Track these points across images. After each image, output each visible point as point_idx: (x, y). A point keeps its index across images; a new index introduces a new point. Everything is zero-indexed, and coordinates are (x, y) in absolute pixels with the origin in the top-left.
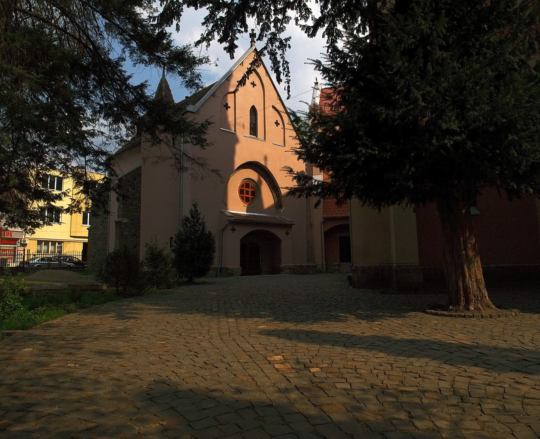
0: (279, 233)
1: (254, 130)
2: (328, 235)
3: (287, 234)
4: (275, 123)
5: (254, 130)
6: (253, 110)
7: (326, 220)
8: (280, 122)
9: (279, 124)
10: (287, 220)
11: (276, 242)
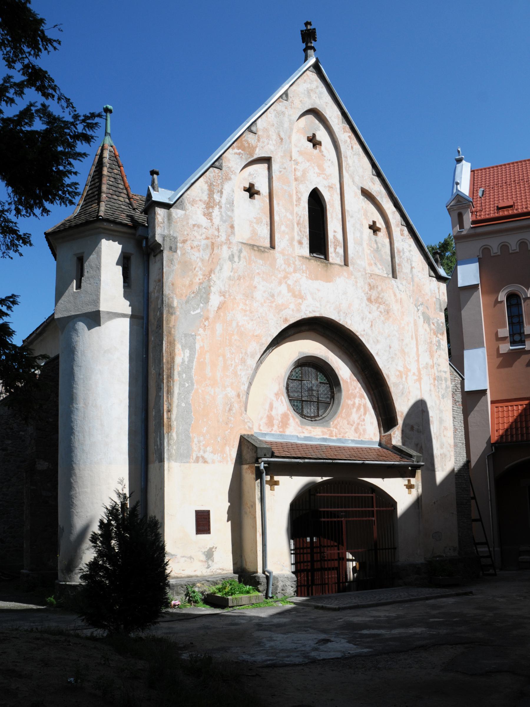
1: (318, 243)
4: (371, 227)
5: (318, 243)
6: (316, 200)
8: (322, 135)
9: (379, 230)
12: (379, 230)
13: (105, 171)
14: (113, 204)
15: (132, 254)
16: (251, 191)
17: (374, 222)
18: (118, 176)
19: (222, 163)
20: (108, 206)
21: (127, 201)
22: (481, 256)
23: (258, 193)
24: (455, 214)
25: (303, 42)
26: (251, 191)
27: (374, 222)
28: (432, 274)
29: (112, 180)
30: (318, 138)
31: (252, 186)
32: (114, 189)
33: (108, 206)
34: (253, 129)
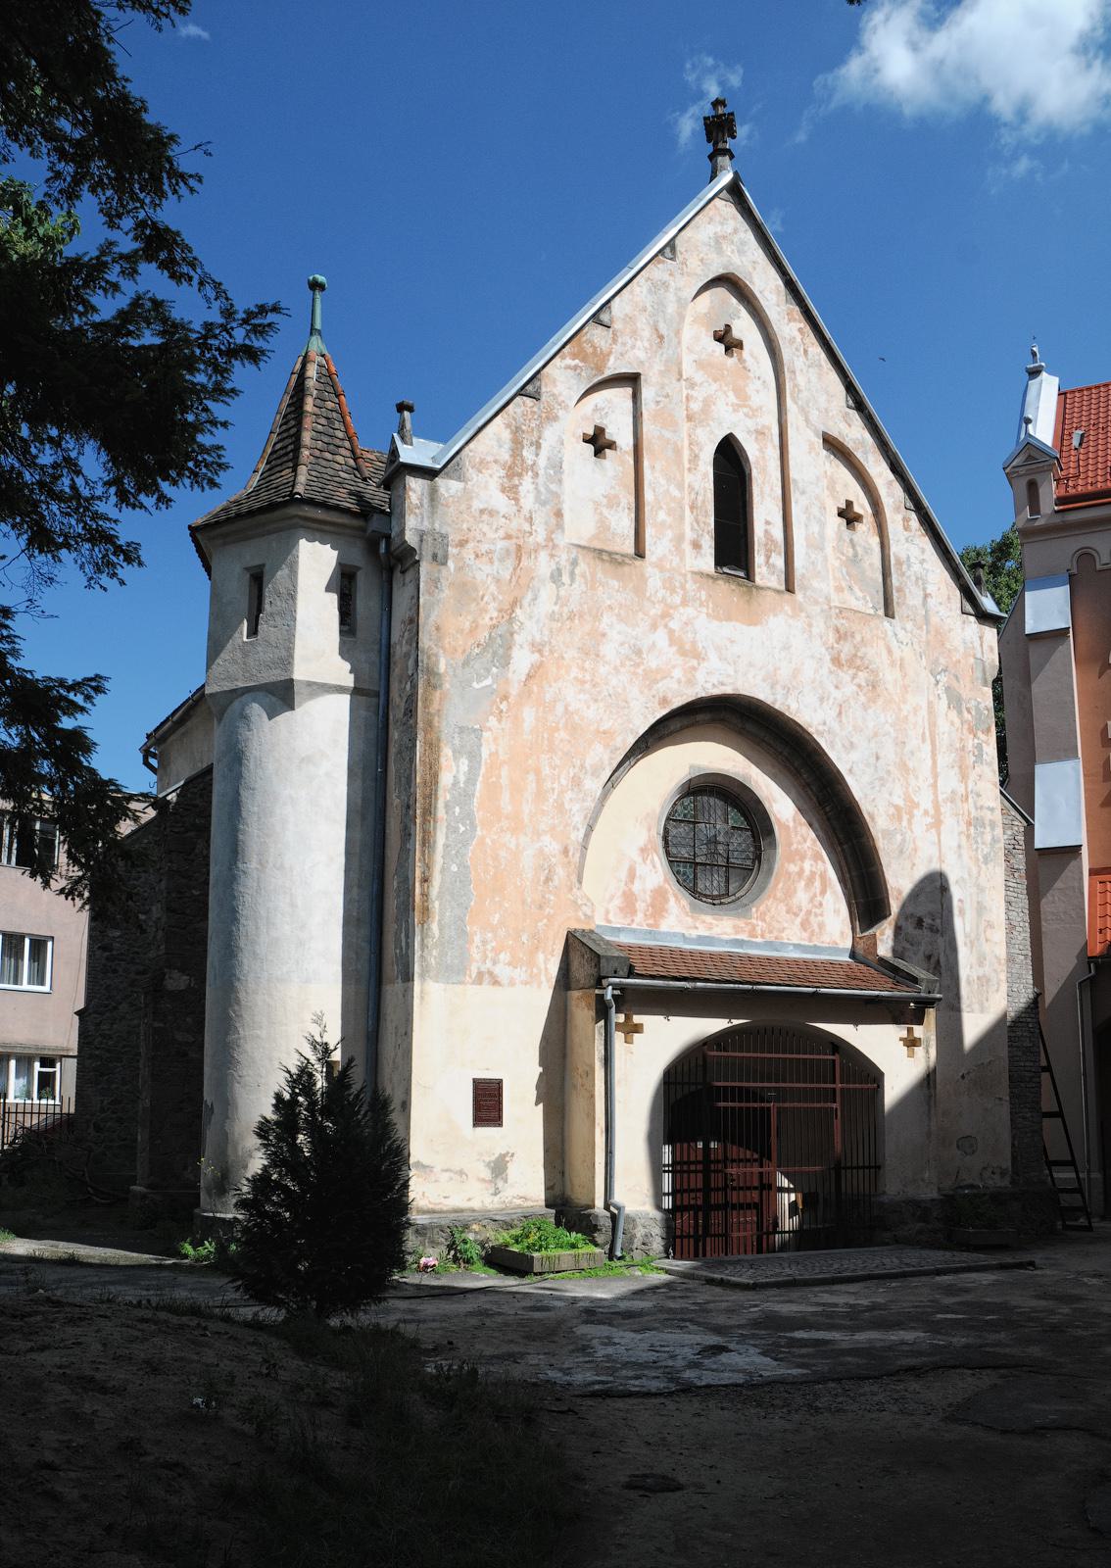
1: (733, 546)
4: (841, 514)
5: (733, 546)
6: (730, 461)
8: (744, 327)
9: (858, 518)
12: (858, 518)
13: (309, 405)
14: (324, 470)
15: (359, 568)
16: (599, 442)
17: (849, 504)
18: (335, 415)
19: (540, 388)
20: (314, 473)
21: (351, 462)
22: (1074, 571)
23: (611, 445)
24: (1023, 483)
25: (709, 141)
26: (599, 442)
27: (849, 504)
28: (969, 608)
29: (323, 421)
30: (736, 333)
31: (599, 431)
32: (326, 439)
33: (314, 473)
34: (604, 317)
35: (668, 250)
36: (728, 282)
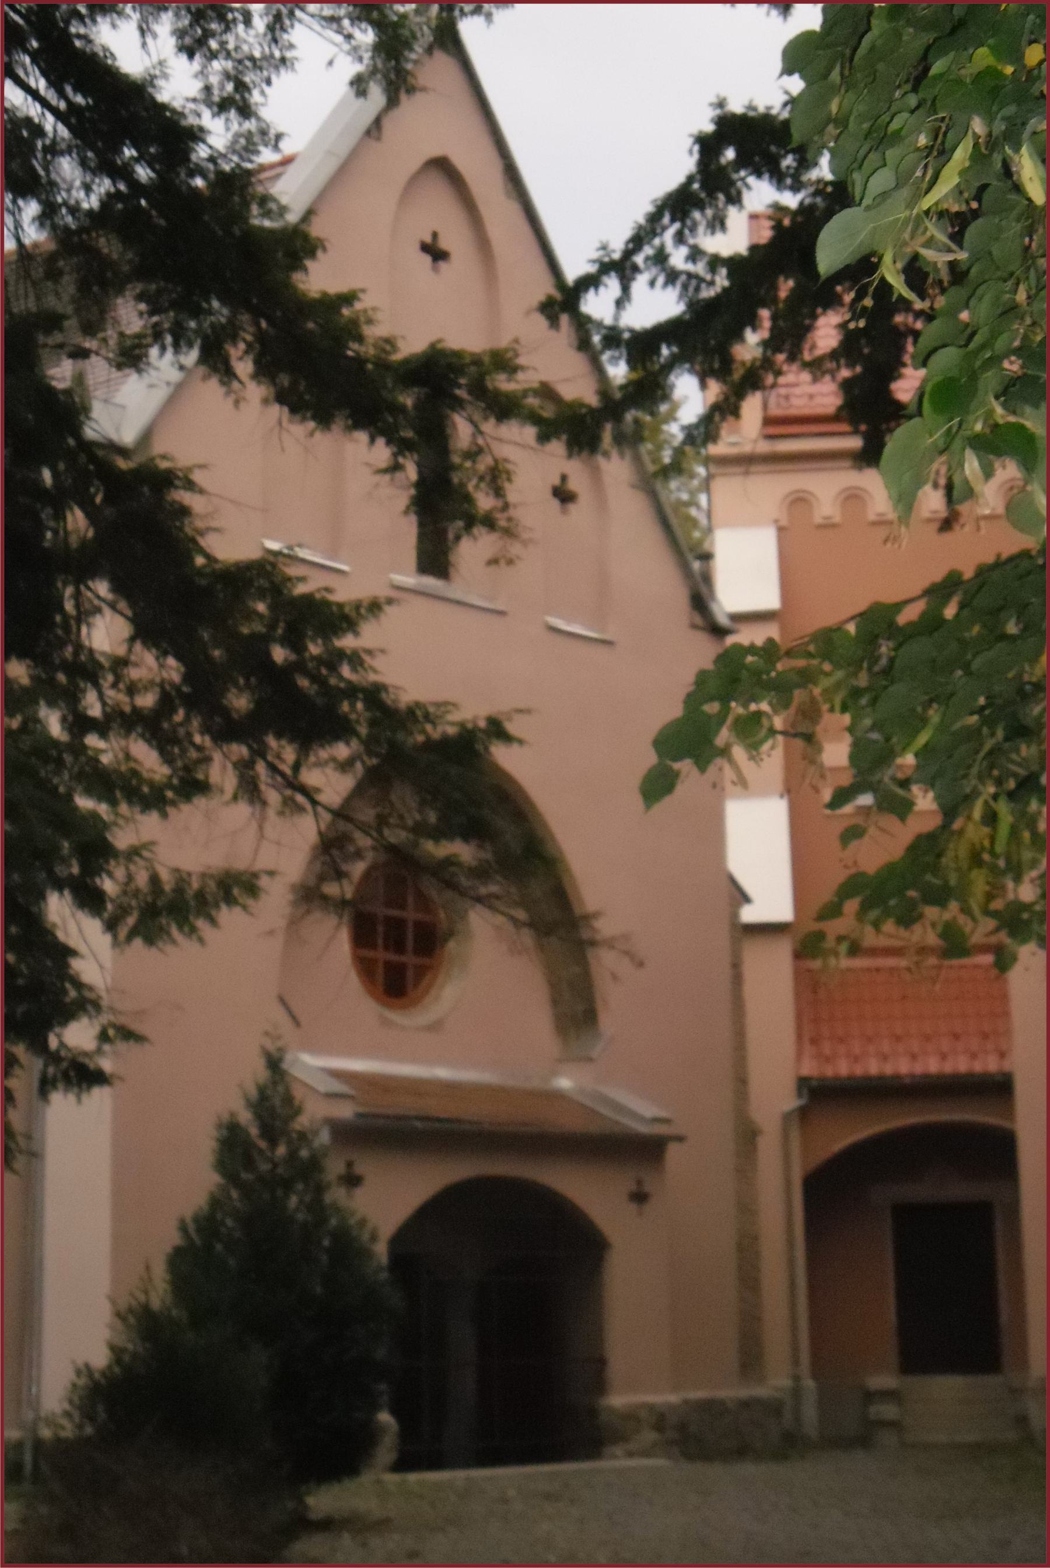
0: (594, 1194)
2: (830, 1192)
3: (640, 1197)
7: (820, 1096)
8: (455, 238)
10: (640, 1109)
11: (579, 1245)
17: (564, 478)
22: (784, 522)
28: (698, 620)
30: (444, 244)
35: (374, 133)
36: (442, 166)
